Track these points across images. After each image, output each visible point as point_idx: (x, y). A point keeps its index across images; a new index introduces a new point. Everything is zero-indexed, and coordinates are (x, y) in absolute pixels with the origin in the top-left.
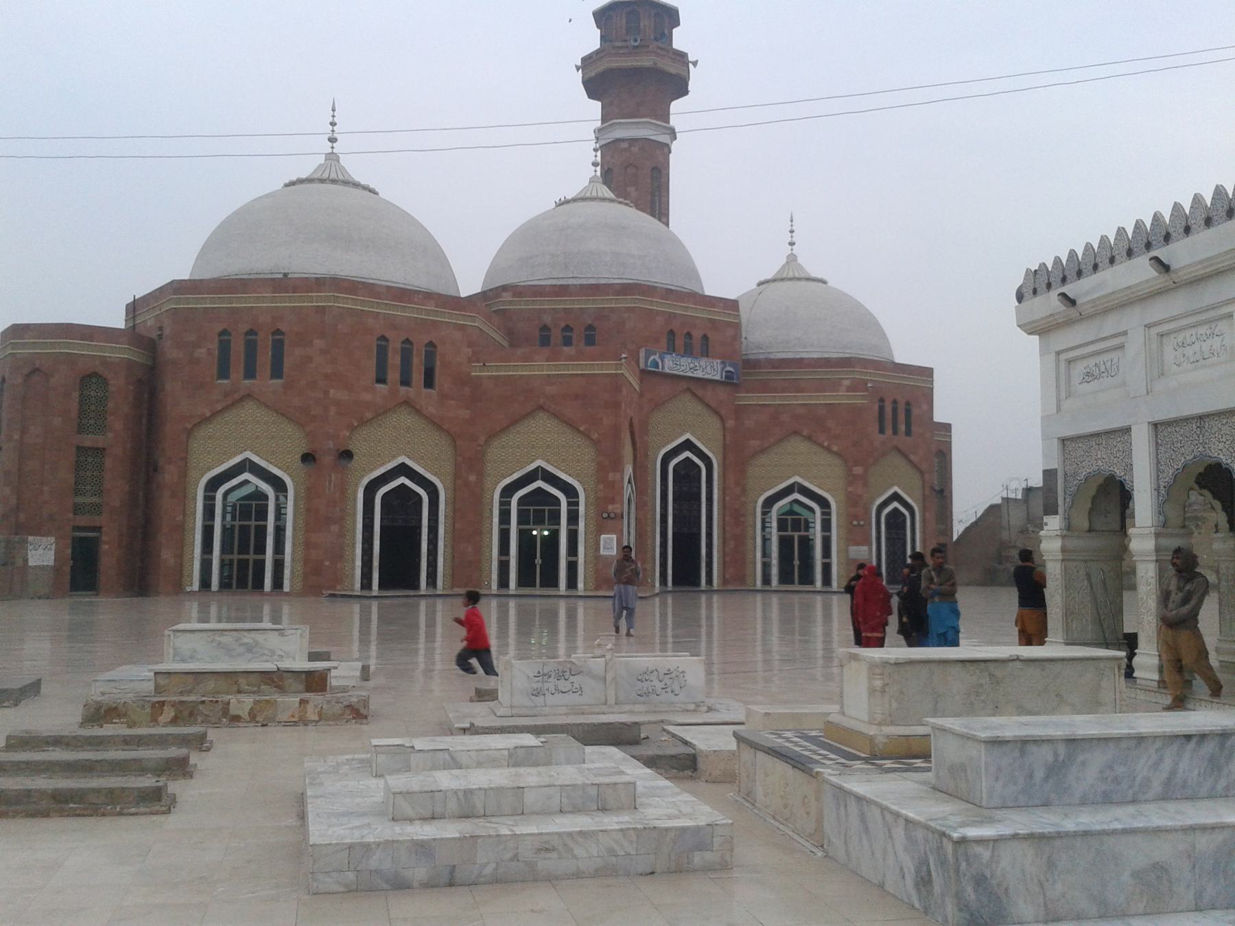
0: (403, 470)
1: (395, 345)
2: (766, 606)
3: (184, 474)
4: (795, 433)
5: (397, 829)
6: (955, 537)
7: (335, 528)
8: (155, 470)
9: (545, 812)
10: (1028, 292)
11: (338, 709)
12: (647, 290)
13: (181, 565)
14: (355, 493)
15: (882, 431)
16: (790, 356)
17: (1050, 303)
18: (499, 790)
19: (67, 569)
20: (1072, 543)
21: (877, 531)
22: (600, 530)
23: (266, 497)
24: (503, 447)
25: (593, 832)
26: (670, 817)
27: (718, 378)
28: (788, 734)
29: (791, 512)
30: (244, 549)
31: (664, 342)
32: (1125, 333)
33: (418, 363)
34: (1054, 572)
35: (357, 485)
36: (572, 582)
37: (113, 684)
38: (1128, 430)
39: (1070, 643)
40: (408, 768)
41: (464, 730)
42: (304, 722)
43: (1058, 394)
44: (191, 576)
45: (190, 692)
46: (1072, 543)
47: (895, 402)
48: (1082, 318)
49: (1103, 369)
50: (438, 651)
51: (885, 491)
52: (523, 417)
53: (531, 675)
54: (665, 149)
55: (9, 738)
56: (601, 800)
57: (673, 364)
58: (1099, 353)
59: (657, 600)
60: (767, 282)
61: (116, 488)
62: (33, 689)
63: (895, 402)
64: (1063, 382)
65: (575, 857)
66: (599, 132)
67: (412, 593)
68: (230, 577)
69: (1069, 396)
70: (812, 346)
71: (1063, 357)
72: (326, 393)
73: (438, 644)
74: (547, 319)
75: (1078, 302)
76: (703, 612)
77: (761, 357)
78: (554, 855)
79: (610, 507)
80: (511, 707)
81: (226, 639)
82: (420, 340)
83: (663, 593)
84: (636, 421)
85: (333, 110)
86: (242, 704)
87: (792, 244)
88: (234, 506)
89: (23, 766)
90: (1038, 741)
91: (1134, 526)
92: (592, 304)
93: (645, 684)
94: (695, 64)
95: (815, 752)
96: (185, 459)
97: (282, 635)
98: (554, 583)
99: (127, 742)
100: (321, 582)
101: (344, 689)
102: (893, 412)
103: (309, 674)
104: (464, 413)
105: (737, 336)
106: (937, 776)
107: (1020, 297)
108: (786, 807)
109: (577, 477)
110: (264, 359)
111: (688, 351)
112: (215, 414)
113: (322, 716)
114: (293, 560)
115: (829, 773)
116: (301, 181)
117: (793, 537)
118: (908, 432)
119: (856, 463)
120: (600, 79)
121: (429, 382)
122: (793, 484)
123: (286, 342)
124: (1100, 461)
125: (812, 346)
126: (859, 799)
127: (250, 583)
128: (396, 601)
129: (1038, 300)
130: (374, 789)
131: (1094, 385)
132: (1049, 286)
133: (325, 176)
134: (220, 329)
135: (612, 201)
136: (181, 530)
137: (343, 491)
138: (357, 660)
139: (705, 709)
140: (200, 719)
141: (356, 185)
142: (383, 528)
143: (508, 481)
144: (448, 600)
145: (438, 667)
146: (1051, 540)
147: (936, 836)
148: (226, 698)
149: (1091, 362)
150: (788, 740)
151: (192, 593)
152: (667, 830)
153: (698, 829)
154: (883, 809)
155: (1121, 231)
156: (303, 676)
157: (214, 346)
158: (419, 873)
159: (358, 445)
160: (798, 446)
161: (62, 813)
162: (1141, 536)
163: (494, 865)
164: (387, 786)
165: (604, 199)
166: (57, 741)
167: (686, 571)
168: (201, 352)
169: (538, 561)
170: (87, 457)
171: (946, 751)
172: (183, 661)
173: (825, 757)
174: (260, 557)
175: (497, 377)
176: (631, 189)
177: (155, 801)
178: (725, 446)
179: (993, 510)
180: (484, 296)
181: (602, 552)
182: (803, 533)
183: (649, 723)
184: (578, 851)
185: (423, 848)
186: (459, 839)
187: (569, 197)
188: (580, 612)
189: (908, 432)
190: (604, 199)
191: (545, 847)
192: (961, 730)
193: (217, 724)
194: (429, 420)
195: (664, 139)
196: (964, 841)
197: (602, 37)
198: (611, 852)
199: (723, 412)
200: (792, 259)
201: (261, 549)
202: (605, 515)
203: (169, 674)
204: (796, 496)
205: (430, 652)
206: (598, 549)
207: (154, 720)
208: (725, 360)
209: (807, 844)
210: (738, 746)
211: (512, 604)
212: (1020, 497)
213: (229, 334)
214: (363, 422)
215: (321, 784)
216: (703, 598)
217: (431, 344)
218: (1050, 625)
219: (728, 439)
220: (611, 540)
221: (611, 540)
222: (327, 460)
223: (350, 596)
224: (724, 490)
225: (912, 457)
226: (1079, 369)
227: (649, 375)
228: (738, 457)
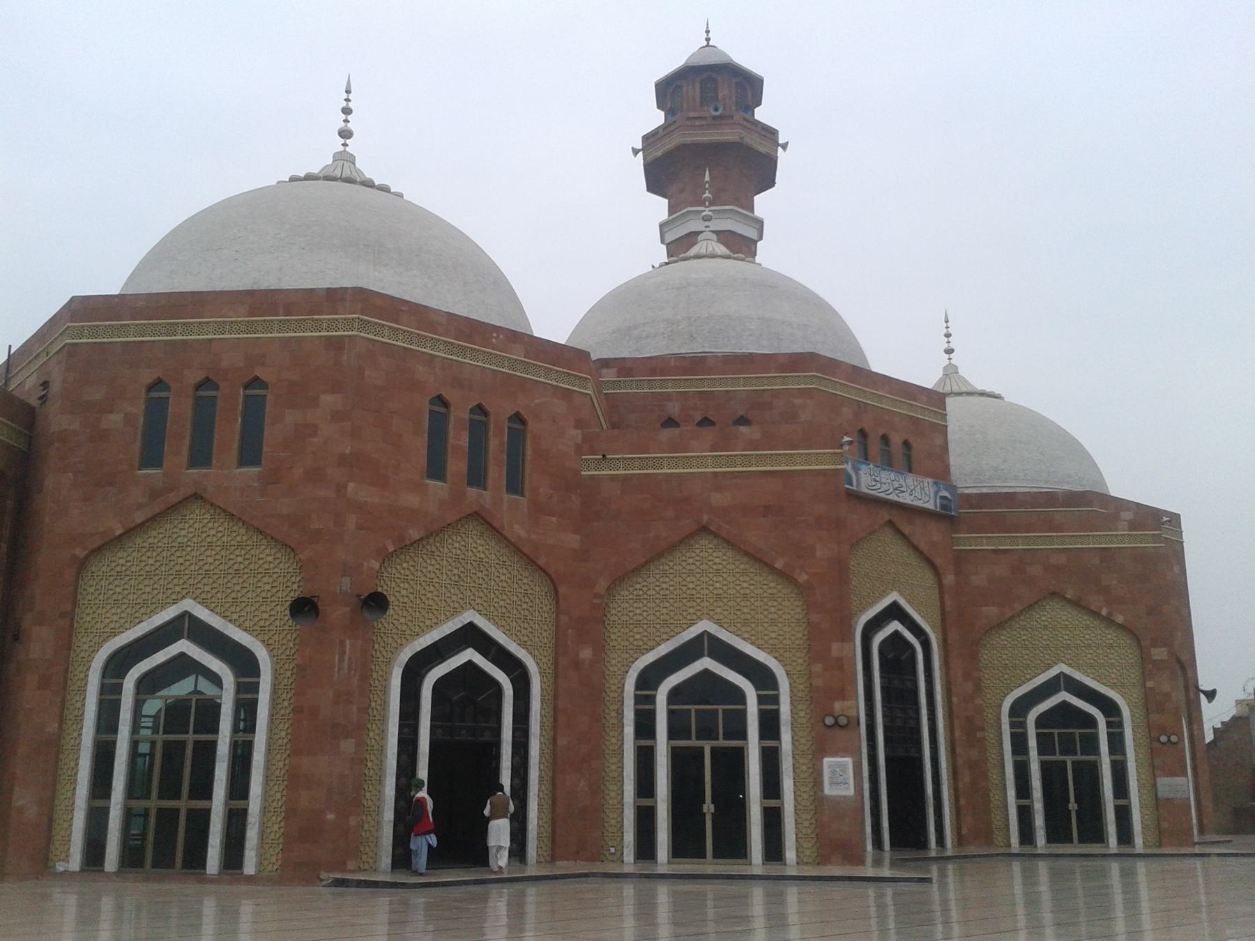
0: (470, 636)
1: (460, 414)
2: (1030, 878)
4: (1053, 594)
7: (348, 746)
8: (16, 638)
13: (51, 820)
14: (386, 679)
24: (638, 600)
35: (389, 662)
36: (774, 850)
44: (67, 840)
52: (672, 547)
57: (873, 480)
70: (1016, 478)
72: (340, 489)
79: (838, 706)
82: (501, 410)
85: (348, 92)
96: (70, 616)
104: (572, 540)
109: (772, 650)
110: (228, 433)
111: (888, 463)
112: (131, 532)
114: (264, 811)
117: (1065, 762)
120: (666, 167)
121: (515, 485)
122: (1057, 677)
134: (147, 376)
136: (53, 751)
137: (365, 677)
142: (887, 759)
157: (137, 409)
159: (396, 588)
160: (1059, 619)
169: (708, 807)
174: (200, 804)
175: (626, 478)
181: (828, 790)
194: (516, 548)
199: (938, 562)
201: (203, 789)
204: (1064, 696)
214: (405, 547)
220: (843, 767)
222: (337, 613)
223: (375, 884)
228: (967, 633)
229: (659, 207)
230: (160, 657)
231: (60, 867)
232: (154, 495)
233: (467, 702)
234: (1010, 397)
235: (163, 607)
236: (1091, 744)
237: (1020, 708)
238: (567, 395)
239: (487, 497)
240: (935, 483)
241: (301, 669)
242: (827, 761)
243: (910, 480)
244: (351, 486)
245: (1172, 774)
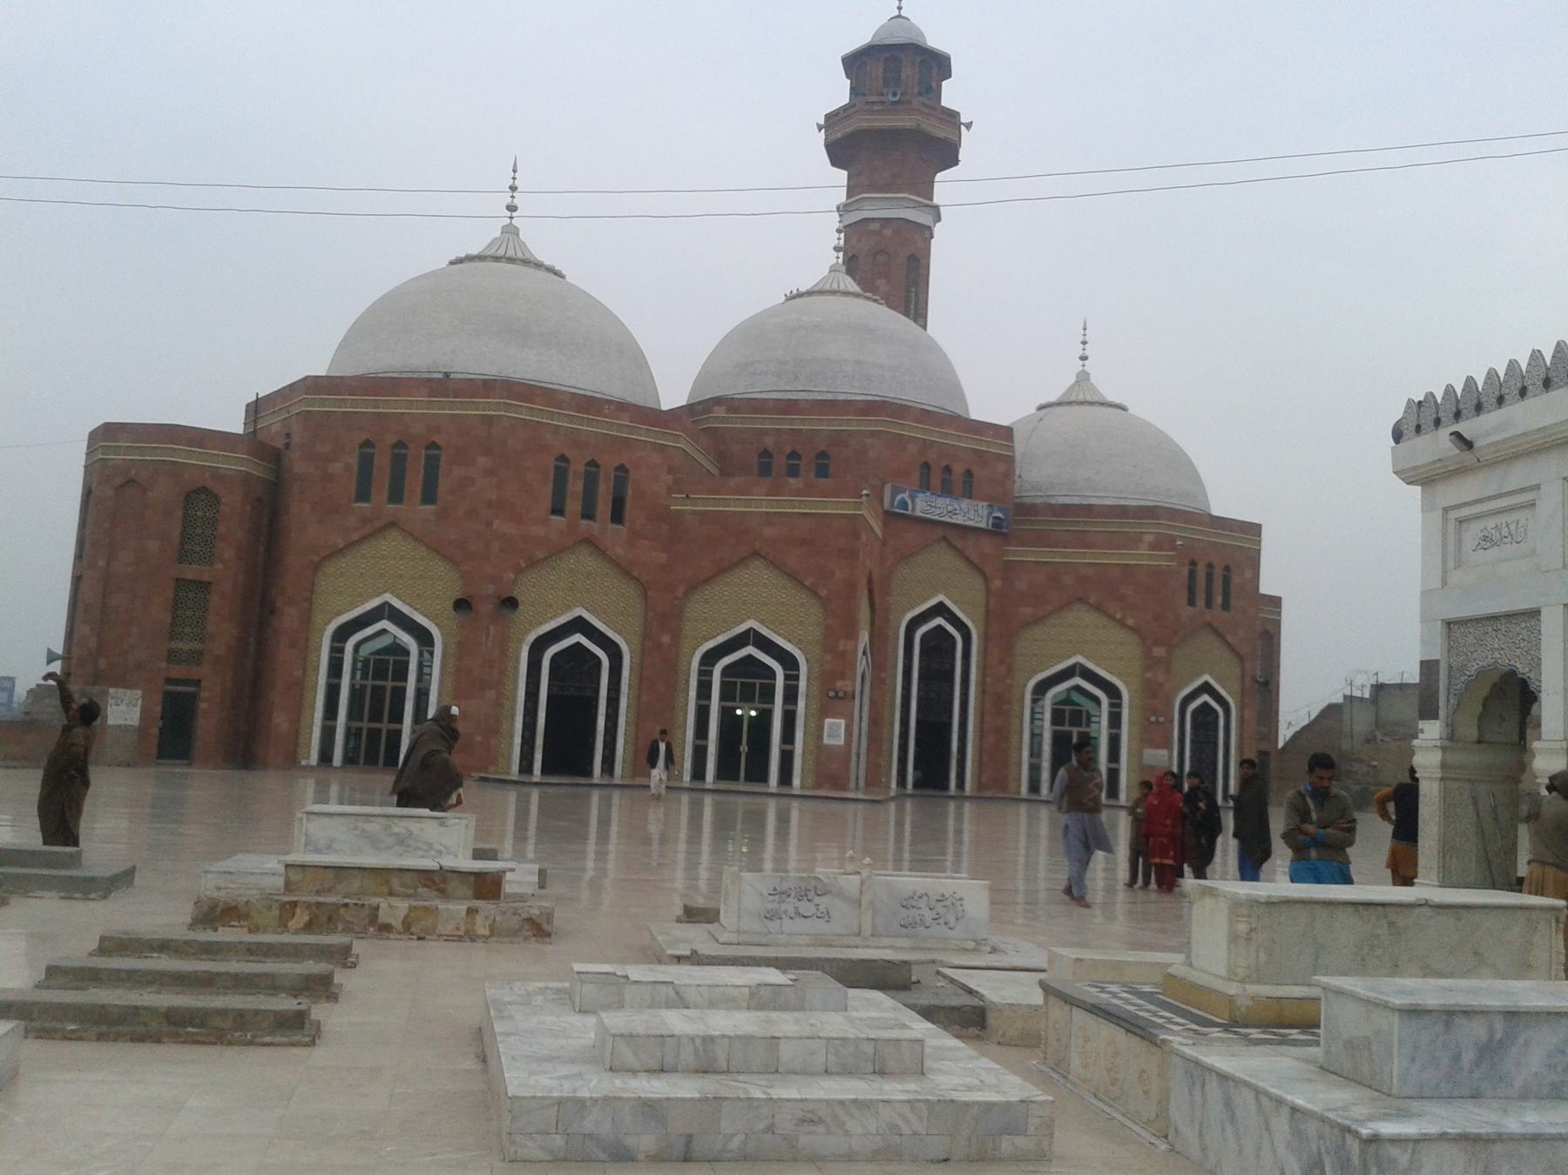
0: (579, 625)
1: (577, 467)
2: (1032, 820)
3: (307, 619)
4: (1080, 600)
5: (618, 1083)
6: (1281, 744)
7: (491, 694)
9: (806, 1072)
10: (1409, 430)
11: (514, 922)
12: (897, 410)
15: (1191, 602)
16: (1076, 501)
17: (1438, 445)
18: (747, 1039)
19: (156, 731)
20: (1456, 758)
21: (1180, 728)
23: (407, 653)
24: (707, 601)
25: (871, 1101)
26: (970, 1088)
27: (982, 525)
28: (1114, 988)
29: (1067, 701)
30: (376, 716)
31: (916, 476)
32: (1537, 487)
33: (604, 491)
34: (1429, 792)
35: (520, 642)
36: (786, 777)
37: (228, 877)
38: (1535, 613)
39: (1444, 884)
40: (621, 1005)
41: (679, 959)
42: (472, 937)
43: (1444, 563)
44: (309, 745)
45: (329, 891)
46: (1456, 758)
47: (1210, 566)
48: (1481, 466)
49: (1505, 532)
50: (612, 856)
51: (1192, 680)
53: (765, 893)
54: (926, 233)
55: (103, 939)
56: (878, 1060)
57: (925, 505)
58: (1499, 512)
59: (892, 806)
60: (1050, 405)
61: (221, 632)
62: (125, 878)
63: (1210, 566)
64: (1451, 548)
65: (846, 1132)
66: (842, 210)
67: (582, 780)
68: (357, 748)
69: (1459, 565)
71: (1453, 515)
72: (489, 524)
73: (611, 847)
74: (769, 442)
75: (1477, 444)
76: (951, 823)
77: (1039, 501)
78: (820, 1129)
79: (839, 684)
80: (738, 932)
81: (373, 827)
82: (609, 462)
83: (901, 797)
84: (876, 577)
86: (395, 909)
87: (1084, 358)
88: (366, 662)
89: (123, 975)
90: (1468, 1013)
91: (1539, 739)
92: (825, 425)
93: (913, 912)
94: (969, 126)
95: (1155, 1014)
96: (310, 601)
97: (442, 825)
98: (763, 777)
99: (253, 951)
101: (521, 898)
102: (1207, 580)
103: (479, 876)
104: (661, 557)
105: (1009, 474)
106: (1328, 1052)
107: (1398, 435)
108: (1114, 1082)
109: (797, 644)
110: (414, 481)
111: (946, 490)
112: (350, 545)
113: (494, 931)
115: (1179, 1040)
116: (470, 259)
118: (1226, 606)
121: (617, 516)
122: (1074, 666)
123: (443, 459)
124: (1496, 653)
126: (1224, 1077)
127: (381, 761)
128: (562, 790)
129: (1420, 441)
130: (583, 1030)
131: (1493, 553)
132: (1438, 422)
133: (501, 253)
135: (857, 295)
136: (299, 689)
138: (531, 861)
139: (988, 949)
140: (340, 927)
141: (539, 265)
142: (918, 722)
143: (710, 644)
144: (628, 792)
145: (611, 874)
146: (1428, 750)
147: (1336, 1131)
148: (374, 901)
149: (1490, 523)
150: (1115, 995)
152: (967, 1104)
153: (1007, 1106)
154: (1258, 1092)
155: (1536, 356)
156: (472, 879)
157: (354, 461)
158: (646, 1142)
159: (526, 591)
160: (1082, 617)
161: (176, 1038)
162: (1550, 751)
163: (741, 1137)
164: (601, 1023)
165: (847, 293)
166: (164, 946)
167: (932, 768)
168: (337, 467)
169: (744, 748)
170: (190, 594)
171: (1341, 1020)
172: (317, 851)
173: (1169, 1020)
174: (396, 726)
176: (881, 283)
177: (295, 1028)
178: (988, 612)
179: (1331, 711)
180: (690, 409)
181: (826, 741)
182: (1083, 729)
183: (922, 963)
184: (851, 1125)
185: (651, 1109)
186: (699, 1100)
187: (803, 289)
188: (795, 816)
189: (1226, 606)
190: (847, 293)
191: (810, 1117)
192: (1360, 994)
193: (361, 934)
195: (922, 218)
196: (1375, 1139)
197: (852, 89)
198: (894, 1129)
200: (1083, 377)
201: (397, 717)
202: (832, 694)
203: (303, 867)
204: (1078, 681)
205: (601, 856)
206: (820, 737)
207: (283, 925)
208: (992, 500)
209: (1144, 1133)
210: (1046, 998)
211: (708, 800)
212: (1367, 695)
214: (533, 563)
215: (510, 1018)
216: (952, 806)
217: (621, 468)
218: (1422, 861)
220: (839, 726)
221: (839, 726)
222: (486, 608)
223: (505, 781)
225: (1230, 639)
226: (1473, 532)
227: (896, 519)
228: (1004, 626)
231: (304, 763)
233: (575, 668)
234: (1133, 410)
235: (371, 597)
236: (768, 694)
238: (663, 448)
239: (594, 527)
242: (828, 721)
243: (965, 504)
244: (496, 523)
245: (1157, 747)
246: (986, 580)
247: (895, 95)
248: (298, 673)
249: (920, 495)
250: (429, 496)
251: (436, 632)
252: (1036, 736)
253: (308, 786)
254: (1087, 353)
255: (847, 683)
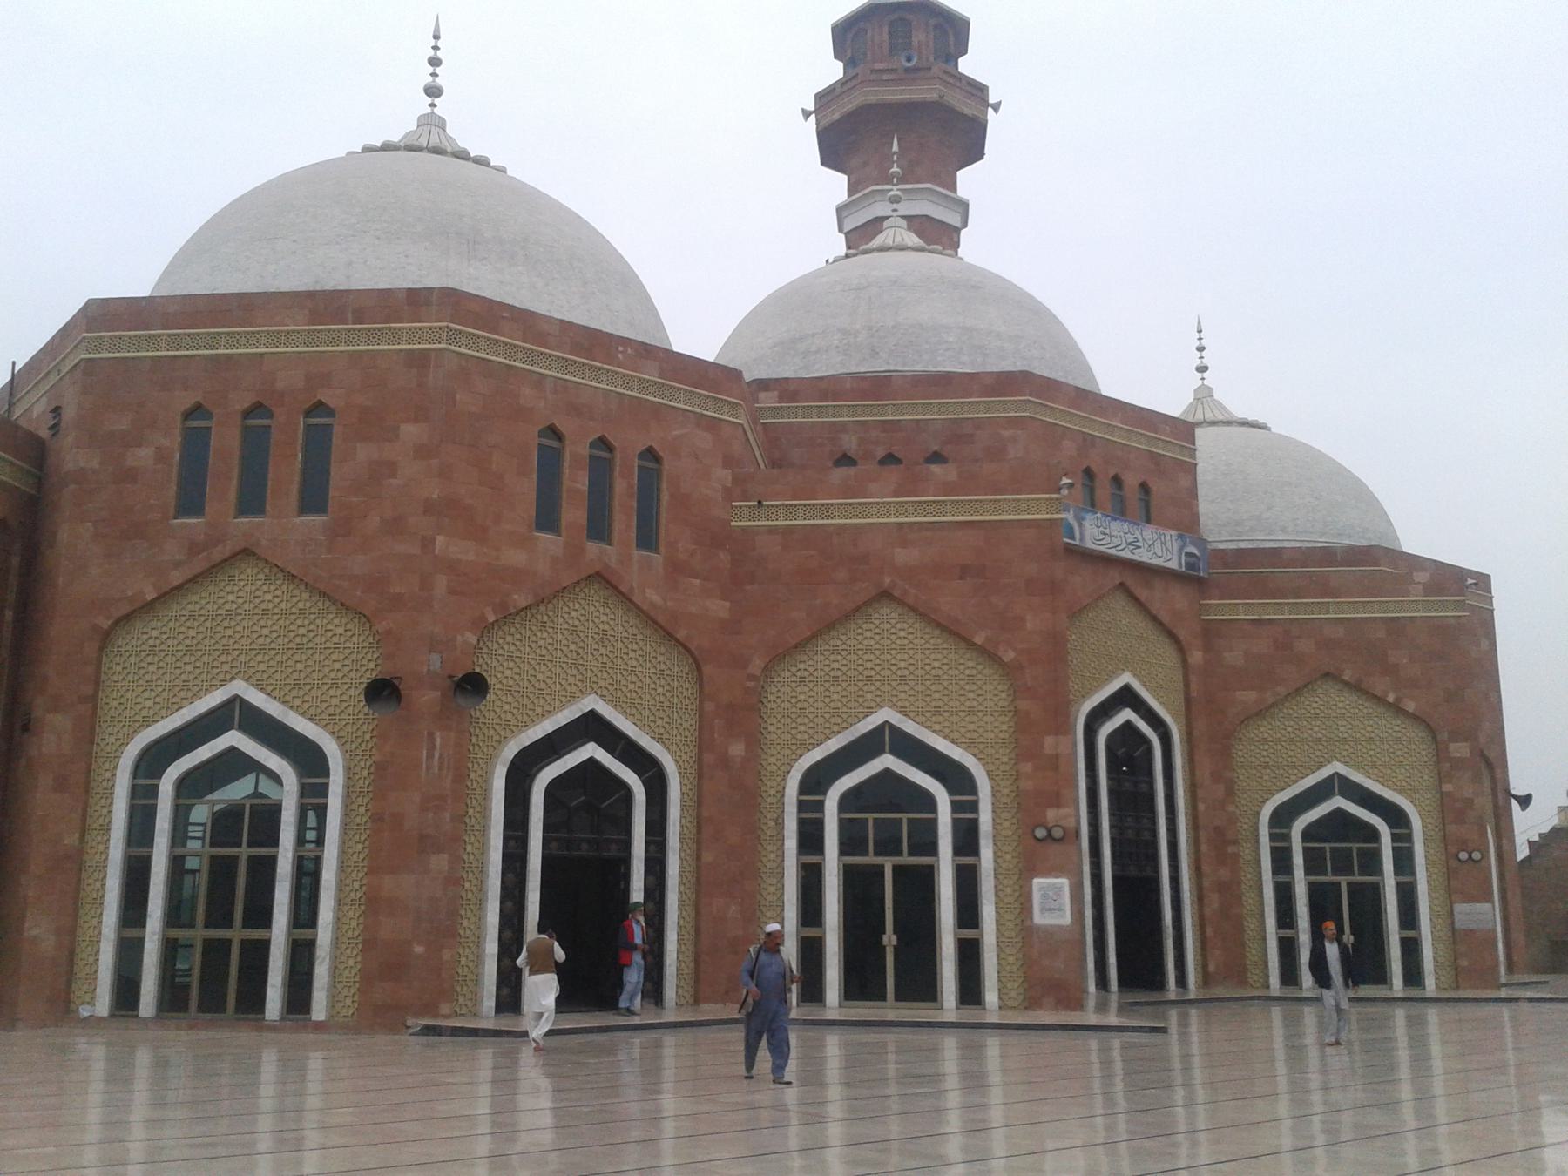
0: (592, 727)
1: (577, 449)
2: (1293, 1025)
3: (87, 733)
7: (439, 862)
8: (26, 728)
13: (72, 953)
14: (487, 779)
22: (1029, 866)
24: (802, 681)
27: (1173, 565)
35: (490, 760)
36: (970, 992)
52: (847, 617)
57: (1101, 533)
70: (1283, 530)
72: (427, 543)
79: (1051, 814)
85: (437, 37)
87: (1202, 369)
100: (405, 996)
104: (719, 608)
109: (970, 745)
110: (285, 474)
111: (1121, 511)
112: (168, 595)
114: (336, 942)
117: (879, 871)
119: (1455, 736)
120: (846, 133)
121: (647, 538)
122: (1331, 778)
123: (337, 430)
125: (1283, 530)
134: (186, 400)
136: (74, 867)
137: (460, 777)
142: (1115, 878)
143: (816, 755)
151: (93, 1022)
157: (172, 442)
159: (496, 666)
160: (1334, 703)
168: (142, 456)
169: (890, 939)
174: (256, 934)
175: (789, 530)
178: (1188, 701)
181: (1039, 918)
194: (648, 618)
195: (952, 219)
199: (1182, 634)
201: (260, 915)
204: (1339, 802)
213: (208, 415)
214: (507, 616)
219: (1193, 686)
220: (1058, 890)
222: (426, 698)
223: (474, 1032)
224: (1192, 789)
228: (1216, 723)
229: (836, 185)
230: (204, 753)
231: (84, 1012)
232: (194, 549)
233: (589, 808)
234: (1279, 426)
237: (1283, 817)
238: (713, 425)
240: (1180, 536)
241: (380, 769)
242: (1037, 882)
243: (1148, 532)
244: (440, 539)
246: (1181, 649)
247: (909, 60)
248: (71, 840)
249: (1089, 516)
250: (313, 498)
251: (330, 747)
252: (811, 881)
253: (95, 1054)
254: (1205, 361)
255: (1063, 811)
